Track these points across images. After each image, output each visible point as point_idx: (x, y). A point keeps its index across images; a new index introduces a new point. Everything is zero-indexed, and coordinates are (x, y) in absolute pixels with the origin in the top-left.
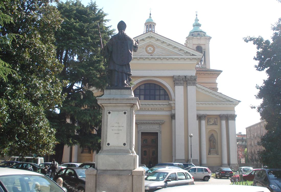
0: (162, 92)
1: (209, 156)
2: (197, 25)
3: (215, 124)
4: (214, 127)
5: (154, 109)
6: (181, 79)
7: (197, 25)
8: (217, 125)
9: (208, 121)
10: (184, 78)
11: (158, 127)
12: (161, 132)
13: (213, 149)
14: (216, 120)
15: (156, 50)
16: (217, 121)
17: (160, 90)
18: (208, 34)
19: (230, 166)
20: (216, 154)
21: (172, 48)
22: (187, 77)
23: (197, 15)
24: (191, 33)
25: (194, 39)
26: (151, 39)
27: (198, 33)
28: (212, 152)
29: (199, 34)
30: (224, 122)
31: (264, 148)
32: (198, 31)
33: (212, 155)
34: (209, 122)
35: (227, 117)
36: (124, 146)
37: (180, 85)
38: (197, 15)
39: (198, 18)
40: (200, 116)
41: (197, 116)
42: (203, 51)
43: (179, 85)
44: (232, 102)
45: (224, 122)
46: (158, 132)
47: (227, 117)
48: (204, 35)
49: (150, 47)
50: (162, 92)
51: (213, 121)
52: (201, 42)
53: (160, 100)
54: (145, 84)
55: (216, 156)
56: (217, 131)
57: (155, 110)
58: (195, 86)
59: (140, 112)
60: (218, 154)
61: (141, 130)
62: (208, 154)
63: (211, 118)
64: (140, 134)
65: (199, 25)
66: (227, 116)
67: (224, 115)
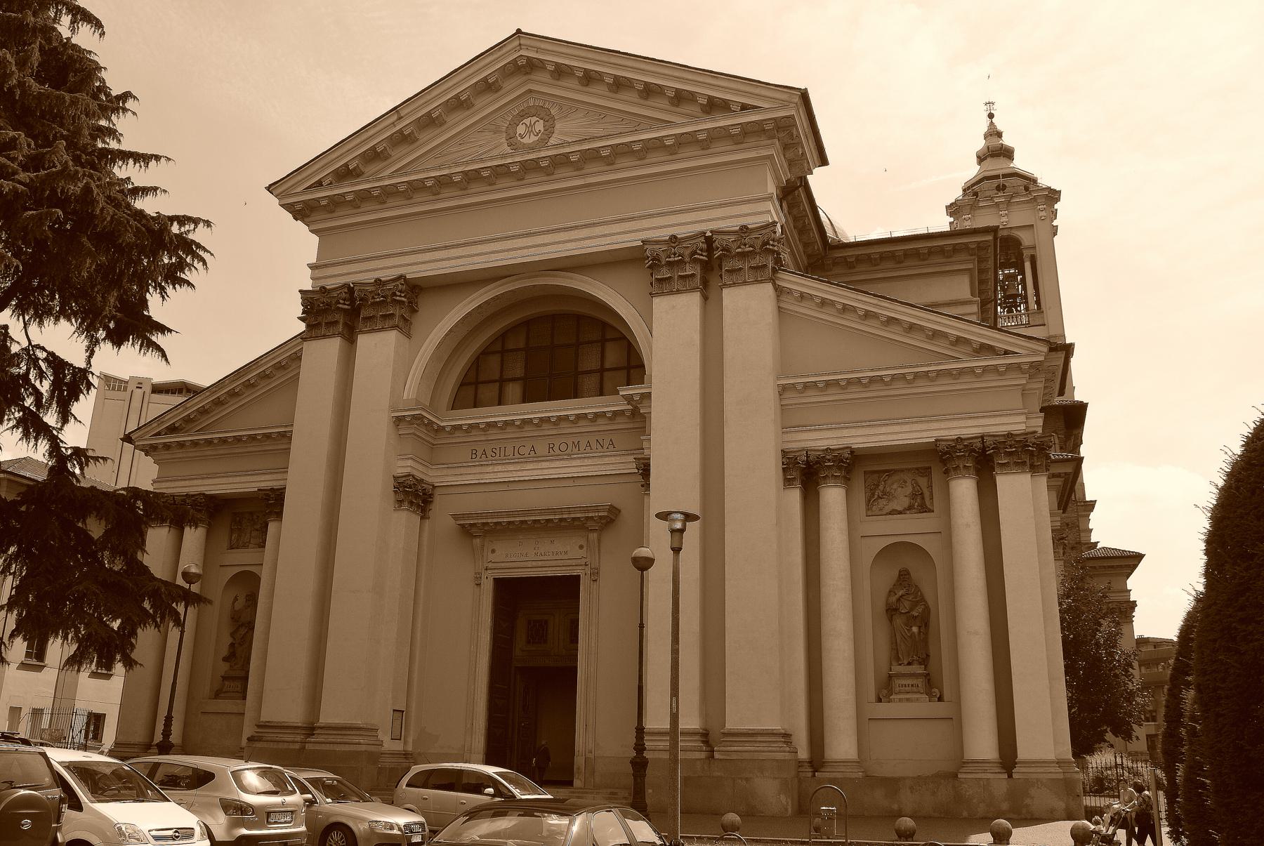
0: (613, 356)
1: (884, 709)
2: (995, 151)
3: (920, 504)
4: (910, 527)
5: (563, 447)
6: (687, 252)
7: (995, 151)
8: (933, 511)
9: (873, 494)
10: (705, 246)
11: (581, 547)
12: (595, 575)
13: (909, 664)
14: (923, 482)
15: (558, 126)
16: (930, 486)
17: (603, 341)
18: (1045, 180)
19: (1010, 776)
20: (930, 694)
21: (636, 100)
22: (719, 241)
23: (991, 116)
24: (969, 188)
25: (978, 211)
26: (532, 77)
27: (995, 182)
28: (904, 682)
29: (1002, 188)
30: (964, 490)
31: (21, 429)
32: (997, 177)
33: (900, 700)
34: (879, 497)
35: (984, 449)
36: (221, 658)
37: (678, 292)
38: (991, 116)
39: (1000, 127)
40: (807, 463)
41: (783, 451)
42: (1026, 253)
43: (671, 293)
44: (1006, 352)
45: (964, 490)
46: (578, 577)
47: (984, 449)
48: (1026, 189)
49: (527, 121)
50: (613, 356)
51: (909, 490)
52: (1012, 219)
53: (601, 394)
54: (527, 324)
55: (922, 707)
56: (930, 545)
57: (569, 451)
58: (769, 287)
59: (490, 469)
60: (940, 699)
61: (490, 565)
62: (880, 700)
63: (890, 473)
64: (488, 586)
65: (1007, 153)
66: (979, 445)
67: (959, 440)
